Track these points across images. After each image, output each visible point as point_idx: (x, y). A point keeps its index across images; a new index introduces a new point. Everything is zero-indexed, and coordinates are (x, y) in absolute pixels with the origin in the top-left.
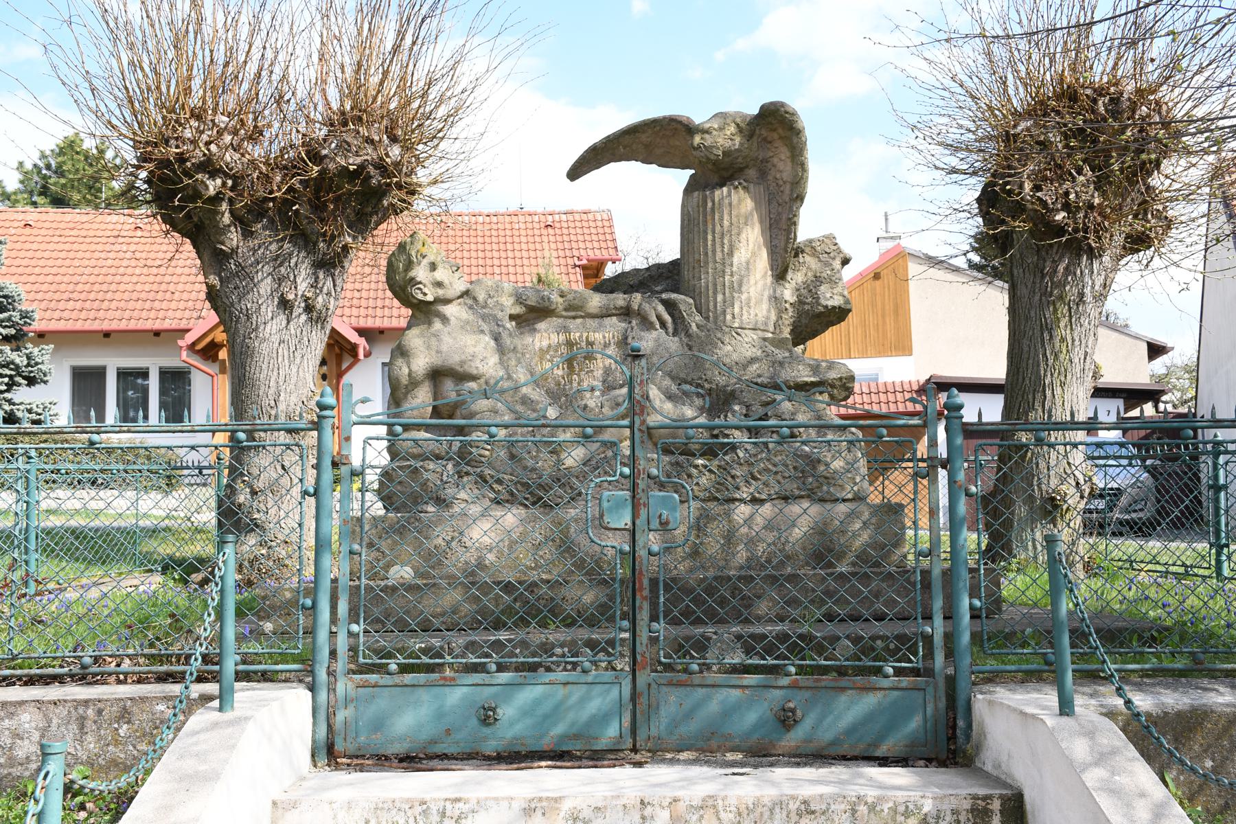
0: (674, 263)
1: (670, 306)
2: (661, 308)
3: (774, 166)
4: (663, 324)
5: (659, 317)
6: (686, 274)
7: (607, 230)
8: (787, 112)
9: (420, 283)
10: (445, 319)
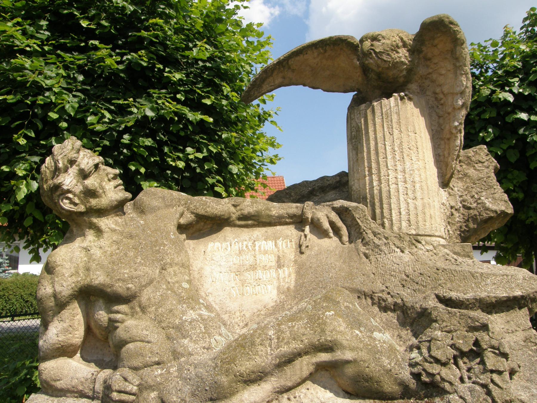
0: (343, 175)
1: (342, 212)
2: (334, 217)
3: (433, 81)
4: (337, 231)
5: (332, 224)
6: (355, 184)
7: (282, 184)
8: (451, 23)
9: (69, 191)
10: (99, 231)
